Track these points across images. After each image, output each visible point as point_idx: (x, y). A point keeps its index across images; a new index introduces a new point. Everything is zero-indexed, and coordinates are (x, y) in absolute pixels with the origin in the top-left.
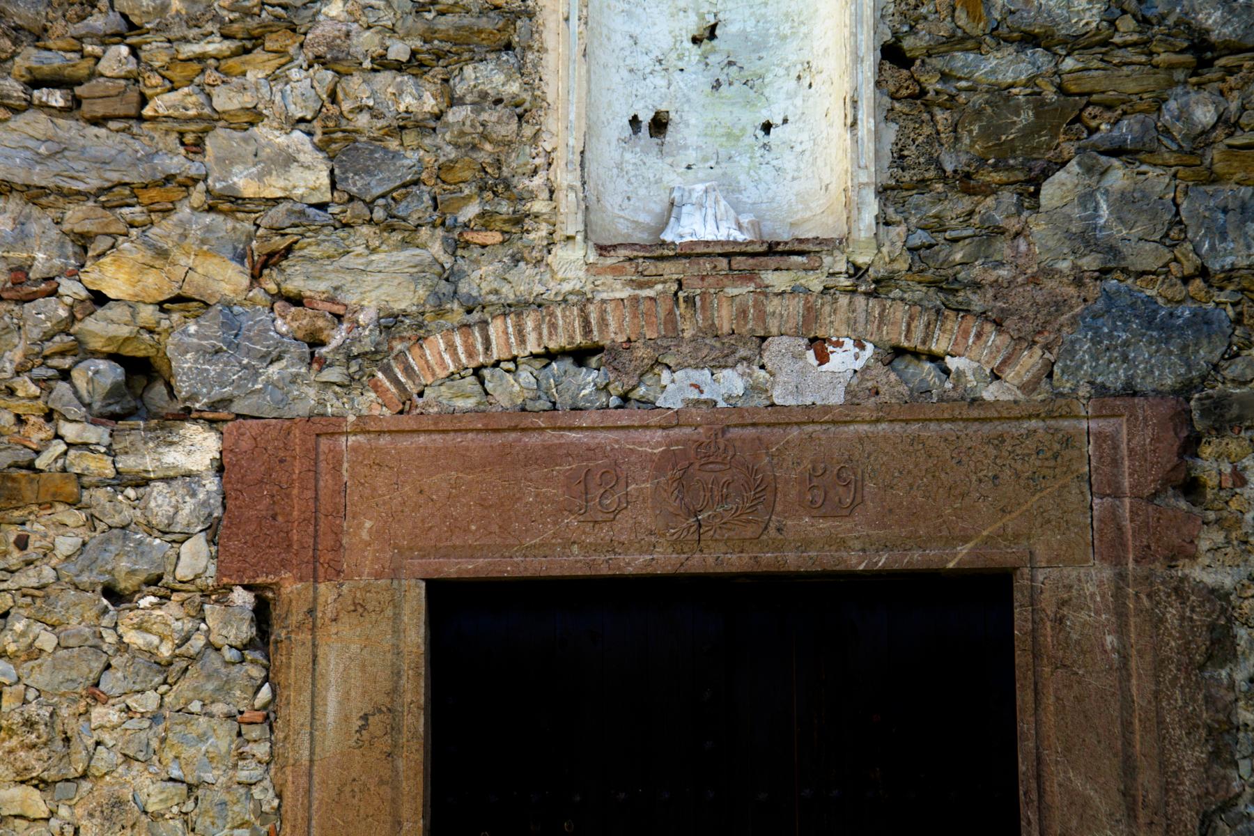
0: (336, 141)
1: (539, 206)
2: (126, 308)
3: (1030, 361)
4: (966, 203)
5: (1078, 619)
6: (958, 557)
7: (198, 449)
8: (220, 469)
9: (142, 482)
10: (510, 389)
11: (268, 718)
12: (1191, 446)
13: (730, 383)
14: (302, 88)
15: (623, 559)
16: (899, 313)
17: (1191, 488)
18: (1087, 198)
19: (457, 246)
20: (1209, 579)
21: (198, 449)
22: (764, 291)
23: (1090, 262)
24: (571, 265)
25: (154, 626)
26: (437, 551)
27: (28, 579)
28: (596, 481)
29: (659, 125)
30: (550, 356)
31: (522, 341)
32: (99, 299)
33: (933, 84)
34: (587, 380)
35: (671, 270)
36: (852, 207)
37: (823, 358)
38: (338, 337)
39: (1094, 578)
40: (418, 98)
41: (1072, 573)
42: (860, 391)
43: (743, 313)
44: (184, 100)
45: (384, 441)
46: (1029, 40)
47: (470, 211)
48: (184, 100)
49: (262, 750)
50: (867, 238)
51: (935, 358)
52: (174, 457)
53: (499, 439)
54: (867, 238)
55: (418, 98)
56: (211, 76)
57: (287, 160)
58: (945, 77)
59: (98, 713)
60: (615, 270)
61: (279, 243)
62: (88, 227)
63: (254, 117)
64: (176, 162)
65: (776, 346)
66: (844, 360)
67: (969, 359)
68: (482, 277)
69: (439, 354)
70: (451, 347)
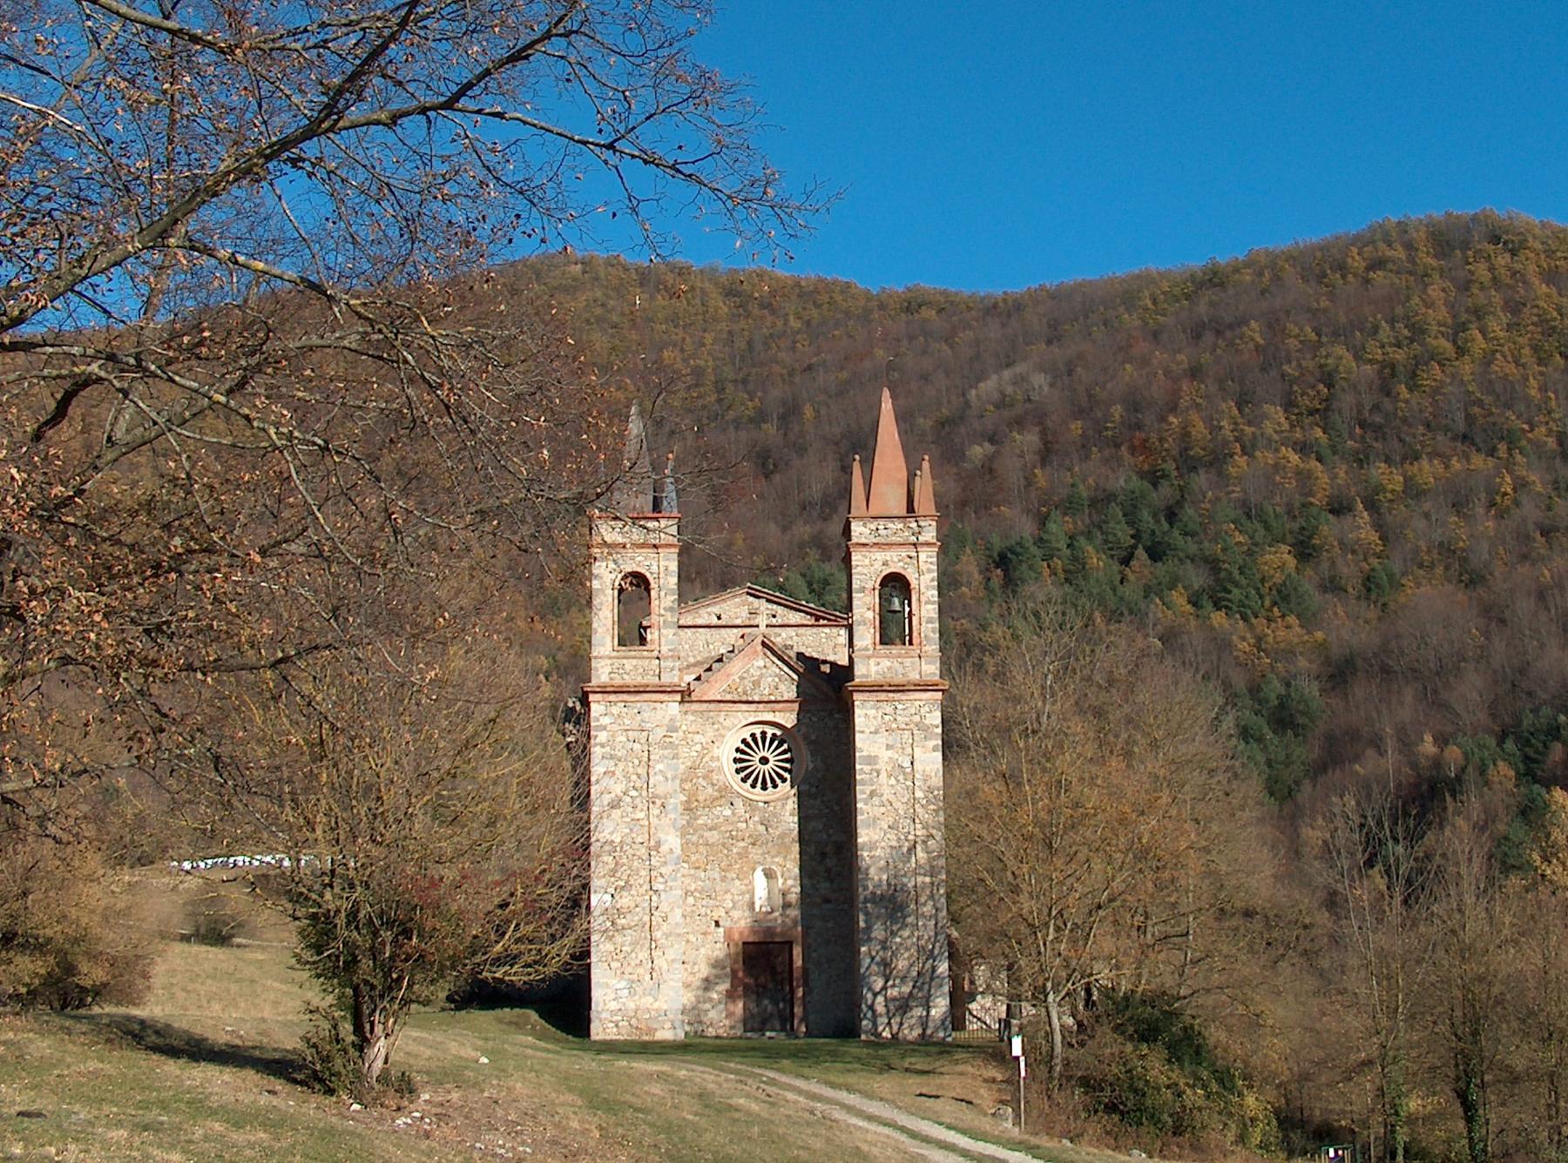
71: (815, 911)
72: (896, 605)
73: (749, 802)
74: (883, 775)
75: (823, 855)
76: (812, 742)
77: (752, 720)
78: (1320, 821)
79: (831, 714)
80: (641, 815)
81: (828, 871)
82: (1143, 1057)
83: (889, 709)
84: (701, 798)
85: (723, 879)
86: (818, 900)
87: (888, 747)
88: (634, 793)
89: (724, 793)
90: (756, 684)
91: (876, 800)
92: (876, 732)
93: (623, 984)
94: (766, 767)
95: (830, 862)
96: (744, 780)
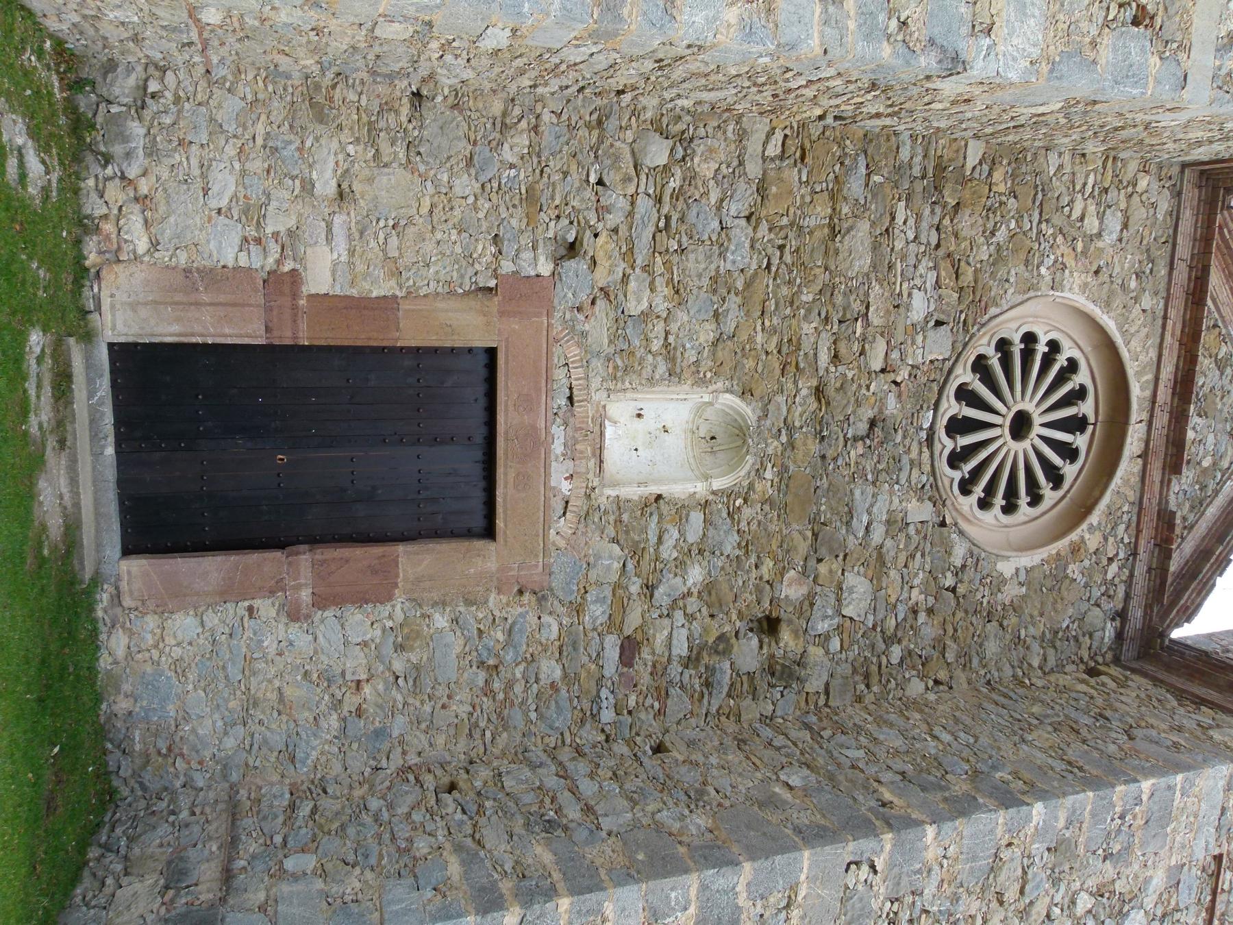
0: (645, 316)
1: (619, 384)
3: (562, 543)
4: (612, 522)
5: (479, 561)
7: (545, 268)
8: (538, 276)
9: (534, 248)
10: (560, 374)
11: (452, 293)
13: (558, 447)
14: (661, 306)
16: (579, 503)
18: (611, 557)
20: (491, 599)
22: (588, 459)
23: (592, 560)
24: (599, 397)
26: (507, 351)
27: (502, 209)
28: (528, 403)
29: (639, 416)
30: (571, 388)
31: (576, 379)
32: (596, 236)
33: (648, 510)
34: (563, 402)
35: (597, 429)
37: (566, 479)
38: (581, 317)
39: (492, 565)
41: (494, 559)
42: (556, 491)
43: (581, 452)
45: (545, 333)
46: (660, 538)
47: (619, 363)
48: (659, 267)
49: (440, 290)
51: (564, 514)
52: (542, 259)
53: (544, 371)
55: (656, 345)
56: (666, 276)
58: (651, 514)
59: (454, 232)
60: (597, 411)
61: (612, 298)
62: (620, 233)
65: (571, 463)
66: (565, 487)
67: (564, 526)
68: (597, 364)
69: (574, 352)
70: (575, 356)
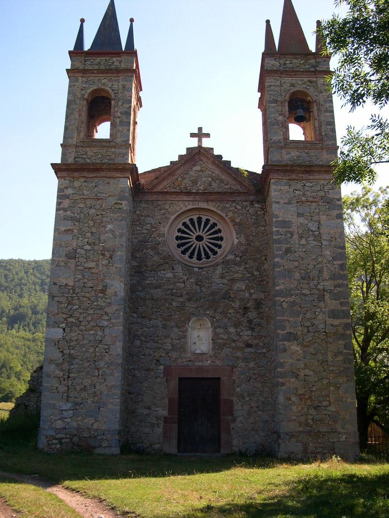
2: (107, 448)
3: (222, 362)
6: (216, 377)
7: (162, 367)
9: (158, 369)
10: (185, 363)
12: (233, 369)
13: (200, 364)
15: (6, 487)
17: (233, 372)
19: (181, 353)
21: (162, 367)
25: (159, 380)
36: (209, 351)
40: (178, 342)
44: (161, 341)
47: (182, 350)
48: (161, 341)
50: (211, 353)
54: (211, 353)
55: (178, 342)
57: (169, 346)
63: (166, 343)
64: (160, 346)
66: (209, 362)
68: (182, 355)
71: (239, 354)
72: (296, 132)
73: (188, 269)
74: (296, 237)
75: (246, 309)
76: (239, 224)
77: (190, 207)
78: (231, 257)
79: (252, 203)
80: (92, 265)
81: (250, 321)
82: (110, 360)
83: (299, 186)
84: (149, 264)
85: (165, 327)
86: (241, 345)
87: (299, 215)
88: (88, 247)
89: (168, 260)
90: (195, 182)
91: (290, 256)
92: (289, 203)
93: (69, 405)
94: (200, 233)
95: (252, 315)
96: (179, 246)
